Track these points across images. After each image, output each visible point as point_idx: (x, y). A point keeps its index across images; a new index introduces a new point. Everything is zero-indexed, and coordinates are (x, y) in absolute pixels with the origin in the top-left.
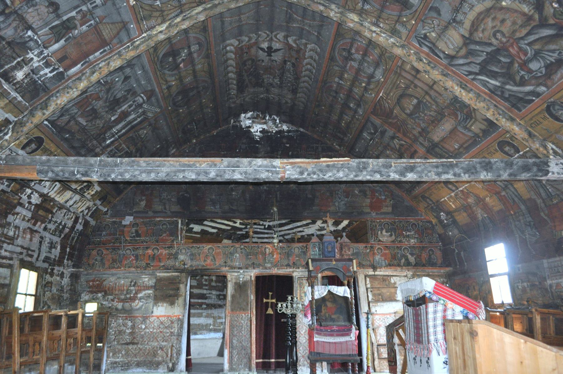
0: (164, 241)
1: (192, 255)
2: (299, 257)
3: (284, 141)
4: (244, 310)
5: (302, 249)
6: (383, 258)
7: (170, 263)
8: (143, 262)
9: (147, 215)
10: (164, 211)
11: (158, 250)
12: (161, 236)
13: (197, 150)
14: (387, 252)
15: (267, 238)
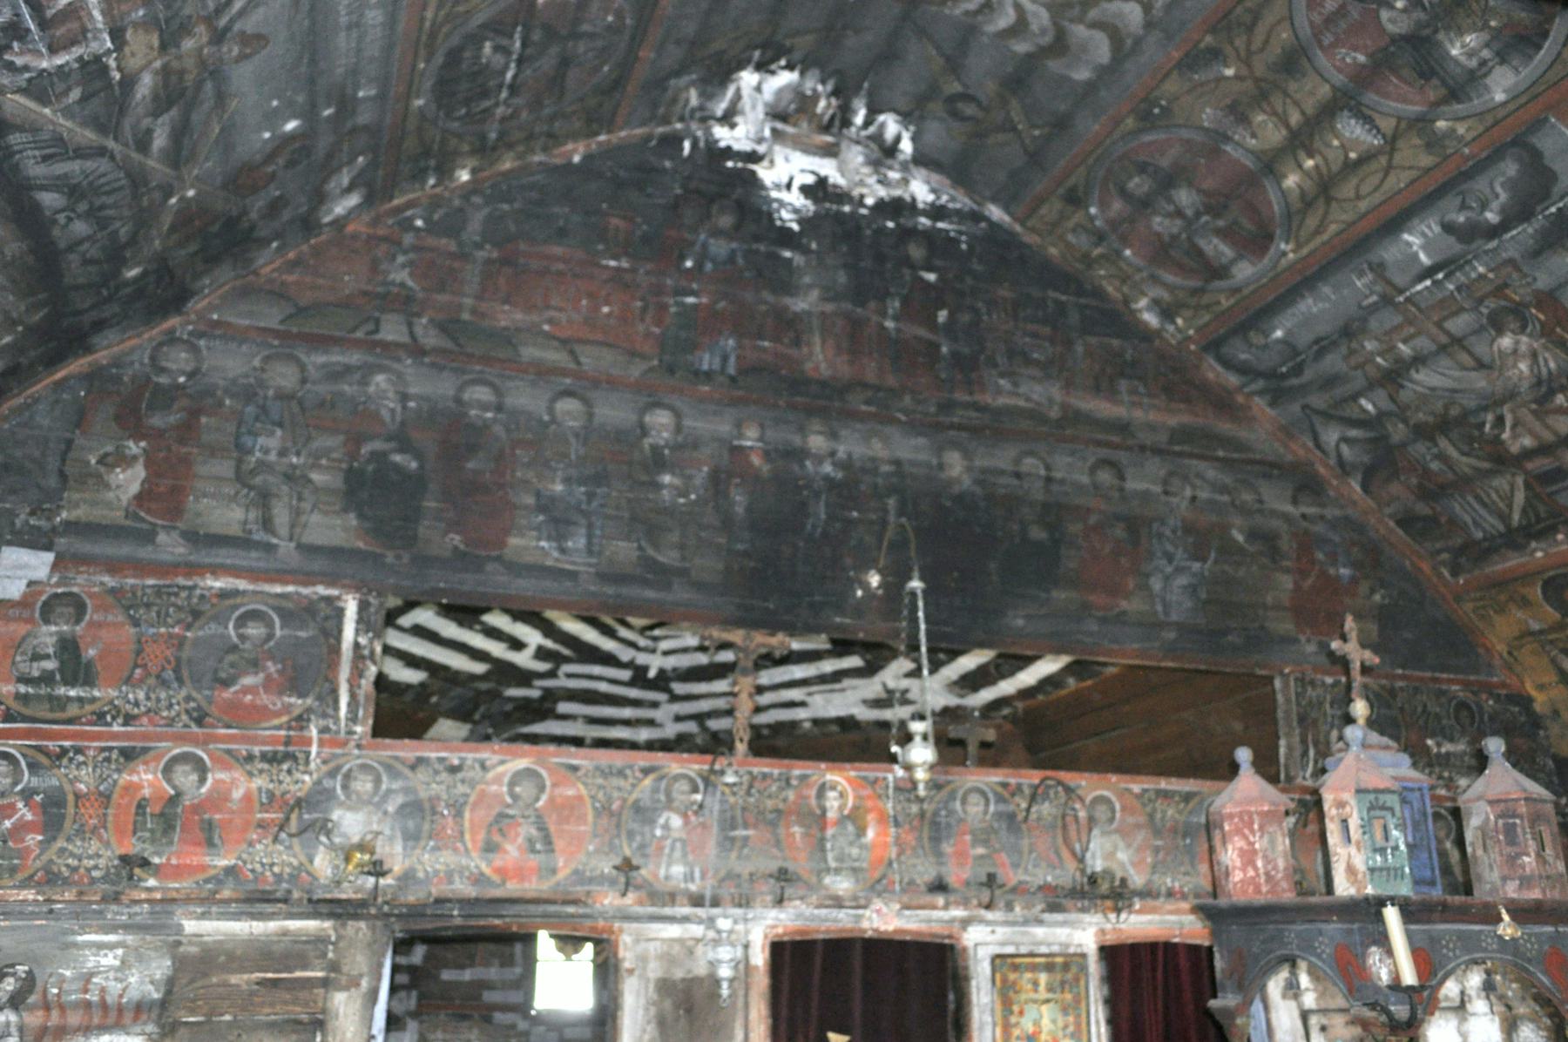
2: (986, 843)
3: (916, 252)
5: (1000, 799)
7: (271, 857)
9: (145, 553)
10: (259, 536)
11: (202, 770)
12: (226, 683)
13: (475, 224)
15: (627, 723)
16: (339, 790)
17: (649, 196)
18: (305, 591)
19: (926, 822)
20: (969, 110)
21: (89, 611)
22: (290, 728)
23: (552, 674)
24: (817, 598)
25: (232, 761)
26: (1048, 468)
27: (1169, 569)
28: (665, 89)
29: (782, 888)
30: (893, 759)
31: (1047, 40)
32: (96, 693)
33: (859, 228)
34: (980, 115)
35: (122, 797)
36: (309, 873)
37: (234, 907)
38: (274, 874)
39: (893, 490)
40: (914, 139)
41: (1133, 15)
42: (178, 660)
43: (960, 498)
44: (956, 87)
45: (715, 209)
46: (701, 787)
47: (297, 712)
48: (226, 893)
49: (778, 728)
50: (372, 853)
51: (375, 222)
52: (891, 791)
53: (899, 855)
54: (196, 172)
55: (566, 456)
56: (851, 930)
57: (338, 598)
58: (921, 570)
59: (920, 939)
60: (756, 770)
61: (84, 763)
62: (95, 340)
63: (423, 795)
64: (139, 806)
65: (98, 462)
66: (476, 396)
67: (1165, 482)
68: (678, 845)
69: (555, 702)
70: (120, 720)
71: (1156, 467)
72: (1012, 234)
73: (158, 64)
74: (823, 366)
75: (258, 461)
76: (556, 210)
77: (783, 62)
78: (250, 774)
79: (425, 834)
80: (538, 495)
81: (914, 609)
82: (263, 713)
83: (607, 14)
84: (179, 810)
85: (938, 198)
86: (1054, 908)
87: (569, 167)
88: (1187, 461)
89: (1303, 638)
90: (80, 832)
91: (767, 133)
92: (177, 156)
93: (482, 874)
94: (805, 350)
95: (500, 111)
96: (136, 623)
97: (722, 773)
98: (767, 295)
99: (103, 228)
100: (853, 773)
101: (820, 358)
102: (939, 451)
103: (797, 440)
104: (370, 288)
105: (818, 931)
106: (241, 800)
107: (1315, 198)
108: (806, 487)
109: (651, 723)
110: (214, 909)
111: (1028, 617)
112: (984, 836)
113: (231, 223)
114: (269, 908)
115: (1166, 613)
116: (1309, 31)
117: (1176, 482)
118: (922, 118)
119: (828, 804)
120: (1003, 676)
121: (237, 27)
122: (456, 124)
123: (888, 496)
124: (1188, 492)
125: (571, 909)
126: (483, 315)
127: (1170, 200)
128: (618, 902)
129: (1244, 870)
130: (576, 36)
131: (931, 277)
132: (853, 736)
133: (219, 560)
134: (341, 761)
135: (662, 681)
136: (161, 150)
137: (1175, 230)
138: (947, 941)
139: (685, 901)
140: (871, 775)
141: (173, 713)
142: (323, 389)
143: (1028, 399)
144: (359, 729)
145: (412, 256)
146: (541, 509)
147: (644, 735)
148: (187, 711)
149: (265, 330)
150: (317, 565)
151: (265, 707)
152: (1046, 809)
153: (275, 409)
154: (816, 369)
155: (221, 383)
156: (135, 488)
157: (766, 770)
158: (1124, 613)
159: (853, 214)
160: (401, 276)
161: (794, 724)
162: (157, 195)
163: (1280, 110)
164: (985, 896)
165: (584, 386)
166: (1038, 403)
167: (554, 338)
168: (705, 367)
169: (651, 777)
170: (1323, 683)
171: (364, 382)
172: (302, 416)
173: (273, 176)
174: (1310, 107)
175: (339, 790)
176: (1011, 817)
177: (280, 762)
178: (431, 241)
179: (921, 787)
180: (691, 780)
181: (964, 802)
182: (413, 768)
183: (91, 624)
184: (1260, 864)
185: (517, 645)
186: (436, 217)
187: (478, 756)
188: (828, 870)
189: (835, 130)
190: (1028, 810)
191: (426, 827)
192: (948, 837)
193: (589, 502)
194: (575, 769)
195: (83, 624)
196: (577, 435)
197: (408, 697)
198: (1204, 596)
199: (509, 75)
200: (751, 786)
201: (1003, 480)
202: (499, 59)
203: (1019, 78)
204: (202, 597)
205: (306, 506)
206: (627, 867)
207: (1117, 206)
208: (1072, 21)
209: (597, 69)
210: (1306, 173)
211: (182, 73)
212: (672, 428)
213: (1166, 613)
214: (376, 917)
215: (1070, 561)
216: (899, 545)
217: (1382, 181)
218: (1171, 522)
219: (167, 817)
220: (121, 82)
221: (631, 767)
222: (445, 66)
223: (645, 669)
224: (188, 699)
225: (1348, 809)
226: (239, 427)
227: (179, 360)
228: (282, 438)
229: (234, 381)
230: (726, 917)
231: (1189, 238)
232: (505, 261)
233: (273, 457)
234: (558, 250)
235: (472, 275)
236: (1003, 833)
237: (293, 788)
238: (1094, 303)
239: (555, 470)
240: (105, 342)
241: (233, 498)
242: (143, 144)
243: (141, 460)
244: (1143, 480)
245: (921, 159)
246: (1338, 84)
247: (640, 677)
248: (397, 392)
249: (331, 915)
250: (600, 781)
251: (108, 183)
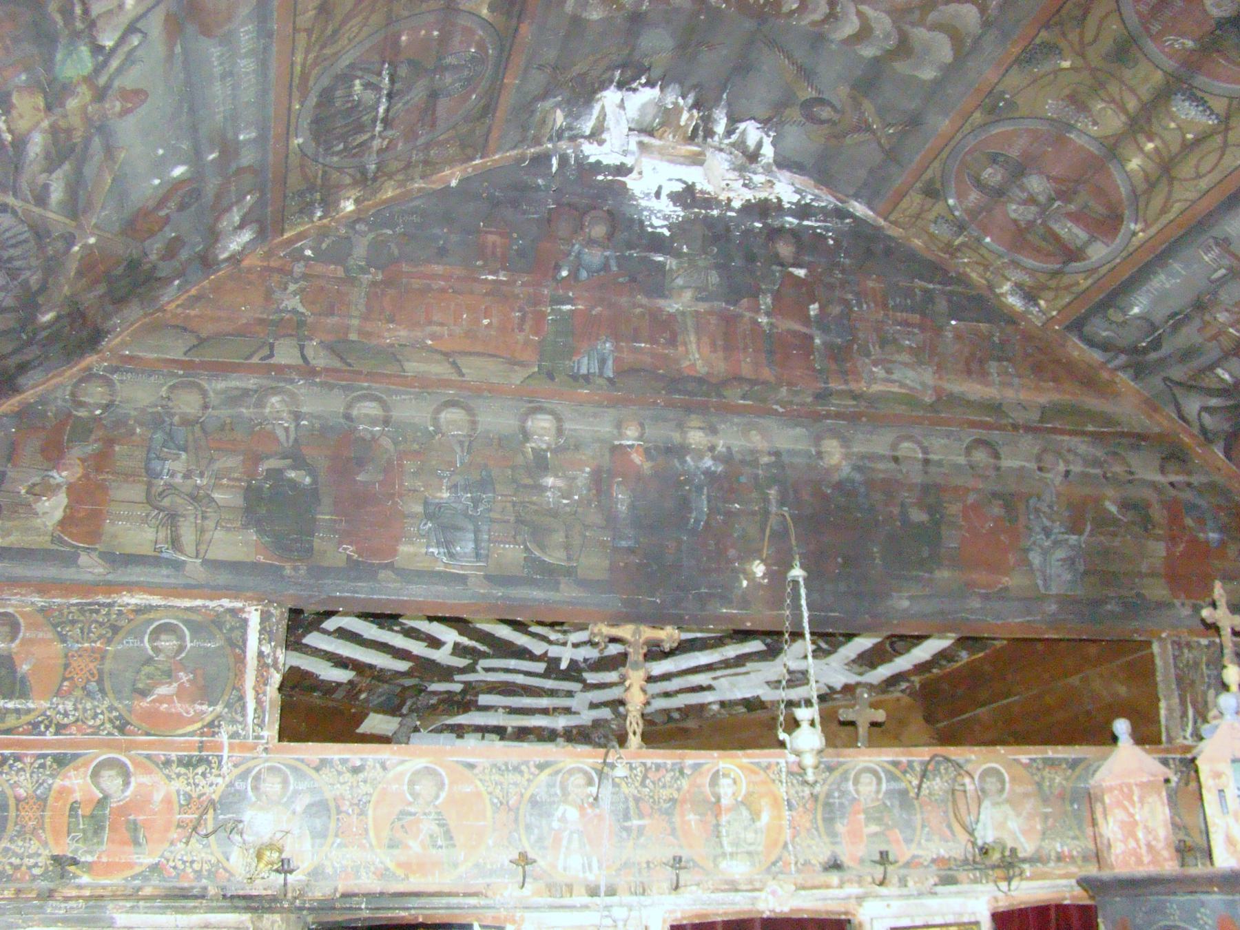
0: (159, 723)
1: (320, 808)
2: (879, 821)
3: (785, 249)
5: (892, 777)
7: (193, 857)
8: (34, 846)
9: (69, 574)
10: (169, 554)
11: (126, 775)
12: (144, 693)
13: (360, 251)
15: (545, 712)
16: (250, 793)
17: (524, 212)
18: (212, 604)
20: (826, 113)
21: (23, 629)
22: (202, 734)
23: (471, 669)
24: (703, 590)
25: (153, 766)
26: (925, 451)
27: (1047, 543)
28: (533, 112)
29: (677, 875)
30: (782, 744)
31: (892, 43)
32: (31, 705)
33: (728, 229)
34: (836, 117)
35: (56, 800)
36: (225, 869)
37: (158, 903)
38: (195, 871)
39: (774, 480)
40: (774, 144)
41: (969, 15)
42: (101, 672)
43: (839, 486)
44: (810, 93)
45: (587, 219)
46: (596, 780)
47: (209, 719)
48: (148, 891)
49: (687, 711)
50: (281, 851)
51: (269, 255)
52: (784, 775)
54: (94, 221)
55: (452, 463)
56: (750, 911)
57: (242, 610)
58: (802, 556)
59: (817, 916)
60: (649, 762)
61: (22, 769)
62: (21, 380)
63: (328, 795)
64: (72, 809)
65: (27, 492)
66: (364, 411)
67: (1039, 458)
68: (575, 836)
69: (477, 695)
70: (52, 730)
71: (1028, 444)
72: (878, 228)
73: (45, 124)
74: (699, 363)
75: (165, 484)
76: (436, 231)
77: (643, 80)
78: (169, 777)
79: (332, 832)
80: (426, 503)
81: (796, 597)
82: (180, 720)
83: (469, 46)
84: (107, 812)
85: (803, 198)
86: (948, 880)
87: (447, 190)
88: (1059, 438)
89: (1177, 602)
90: (21, 834)
91: (633, 146)
92: (75, 206)
93: (387, 869)
94: (681, 349)
95: (376, 144)
96: (64, 641)
97: (613, 766)
98: (641, 299)
99: (13, 279)
100: (745, 760)
101: (696, 356)
102: (818, 439)
103: (676, 437)
104: (265, 316)
105: (718, 915)
106: (162, 801)
107: (1158, 180)
108: (687, 482)
109: (567, 711)
110: (141, 903)
111: (910, 598)
112: (877, 815)
113: (133, 265)
114: (191, 904)
115: (1047, 587)
116: (1136, 19)
117: (1049, 459)
118: (781, 123)
119: (722, 791)
120: (899, 653)
121: (116, 84)
122: (335, 159)
123: (769, 488)
124: (1062, 467)
125: (473, 901)
126: (369, 335)
127: (1022, 188)
128: (517, 893)
129: (1125, 841)
130: (442, 69)
131: (801, 272)
132: (760, 714)
133: (134, 579)
134: (251, 764)
135: (574, 672)
136: (60, 203)
137: (1030, 217)
138: (843, 917)
139: (583, 891)
140: (764, 761)
141: (98, 722)
142: (225, 413)
143: (902, 385)
144: (265, 733)
145: (303, 283)
146: (429, 516)
147: (560, 722)
148: (111, 721)
149: (174, 361)
150: (223, 578)
151: (180, 715)
152: (937, 785)
153: (181, 434)
154: (693, 365)
155: (133, 413)
156: (59, 515)
157: (659, 761)
158: (1006, 589)
159: (721, 218)
160: (293, 303)
161: (702, 707)
162: (60, 245)
163: (1117, 98)
164: (879, 871)
165: (467, 396)
166: (912, 389)
167: (436, 351)
168: (584, 371)
169: (548, 771)
171: (260, 404)
172: (205, 438)
173: (167, 219)
174: (1145, 93)
175: (250, 793)
176: (904, 793)
177: (195, 766)
178: (319, 268)
179: (810, 771)
180: (586, 773)
181: (856, 782)
182: (317, 769)
183: (24, 642)
184: (1140, 835)
185: (435, 643)
186: (324, 246)
187: (379, 757)
188: (724, 855)
189: (699, 140)
190: (919, 787)
191: (333, 825)
192: (842, 817)
193: (476, 507)
194: (471, 766)
195: (17, 642)
196: (461, 443)
197: (339, 695)
198: (1082, 568)
199: (381, 110)
200: (645, 777)
201: (881, 466)
202: (370, 96)
203: (868, 81)
204: (120, 613)
205: (210, 524)
206: (524, 860)
207: (974, 196)
208: (913, 24)
209: (466, 98)
210: (1147, 156)
211: (69, 131)
212: (553, 431)
213: (1047, 587)
214: (289, 910)
215: (951, 540)
216: (780, 536)
217: (1221, 158)
218: (1047, 497)
219: (97, 819)
220: (13, 143)
221: (526, 763)
222: (319, 105)
223: (557, 660)
224: (111, 708)
225: (1224, 778)
226: (149, 451)
227: (95, 394)
228: (188, 461)
229: (143, 410)
230: (621, 905)
231: (1044, 223)
232: (388, 283)
233: (178, 479)
234: (438, 269)
235: (358, 297)
236: (896, 811)
237: (208, 790)
238: (960, 289)
239: (441, 478)
240: (31, 383)
241: (145, 520)
242: (41, 199)
243: (64, 488)
244: (1017, 457)
245: (783, 163)
246: (1170, 71)
247: (553, 668)
248: (290, 412)
249: (248, 909)
250: (497, 777)
251: (15, 236)
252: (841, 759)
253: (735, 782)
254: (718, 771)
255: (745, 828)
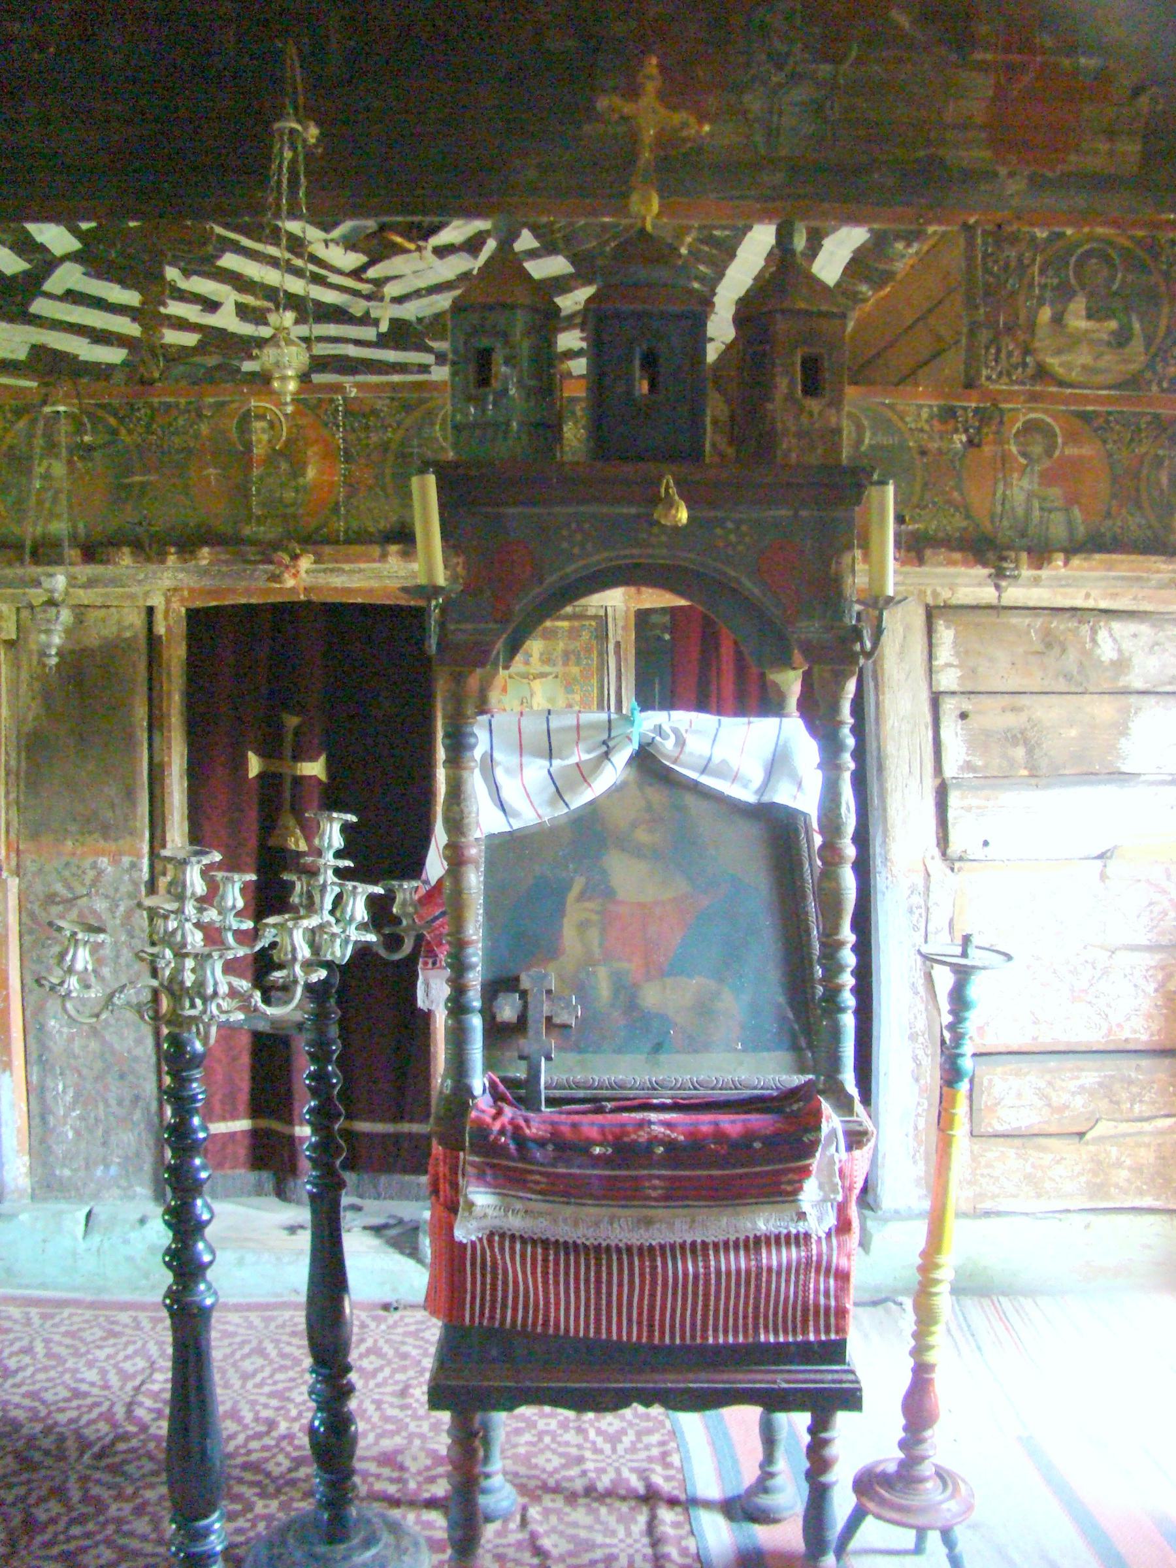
4: (106, 831)
6: (1055, 492)
14: (1086, 451)
19: (391, 457)
53: (348, 497)
89: (1003, 171)
170: (1033, 238)
185: (212, 306)
252: (425, 395)
253: (272, 425)
254: (249, 410)
255: (283, 486)
